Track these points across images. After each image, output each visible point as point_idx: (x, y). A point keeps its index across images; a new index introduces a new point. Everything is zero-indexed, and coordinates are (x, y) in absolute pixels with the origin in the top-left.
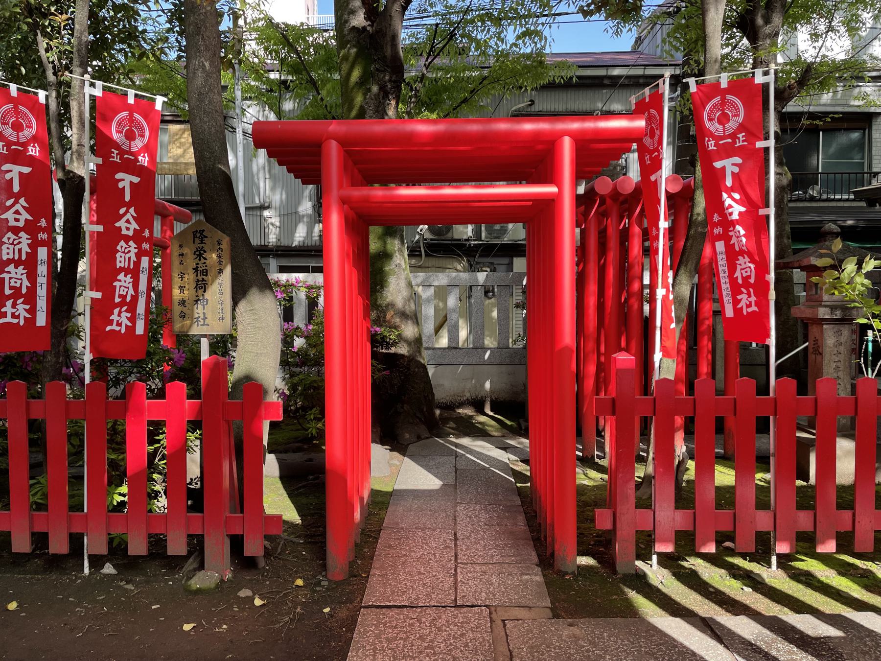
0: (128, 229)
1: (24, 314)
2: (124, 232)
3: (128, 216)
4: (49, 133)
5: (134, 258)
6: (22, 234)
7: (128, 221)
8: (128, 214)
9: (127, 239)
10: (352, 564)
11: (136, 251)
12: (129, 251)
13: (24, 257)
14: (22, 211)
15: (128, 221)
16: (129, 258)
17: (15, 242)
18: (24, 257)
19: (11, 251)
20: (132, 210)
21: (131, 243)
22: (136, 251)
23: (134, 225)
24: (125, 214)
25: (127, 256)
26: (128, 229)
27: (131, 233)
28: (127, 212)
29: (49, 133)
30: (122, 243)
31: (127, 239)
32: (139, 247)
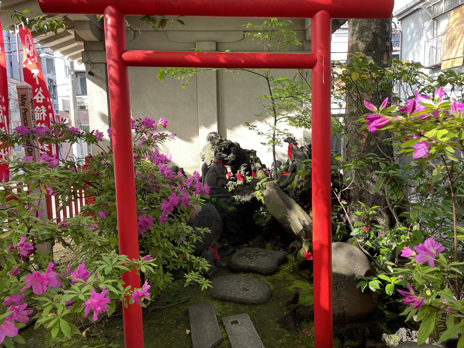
0: (40, 99)
1: (46, 149)
2: (38, 101)
3: (39, 93)
4: (406, 149)
5: (45, 115)
6: (42, 107)
7: (39, 95)
8: (39, 91)
9: (40, 105)
10: (283, 186)
11: (46, 110)
12: (42, 111)
13: (44, 119)
14: (41, 95)
15: (39, 95)
16: (42, 115)
17: (40, 111)
18: (44, 119)
19: (38, 116)
20: (40, 89)
21: (42, 107)
22: (46, 110)
23: (43, 97)
24: (38, 92)
25: (41, 114)
26: (40, 99)
27: (41, 101)
28: (39, 90)
29: (406, 149)
30: (37, 107)
31: (40, 105)
32: (47, 108)
